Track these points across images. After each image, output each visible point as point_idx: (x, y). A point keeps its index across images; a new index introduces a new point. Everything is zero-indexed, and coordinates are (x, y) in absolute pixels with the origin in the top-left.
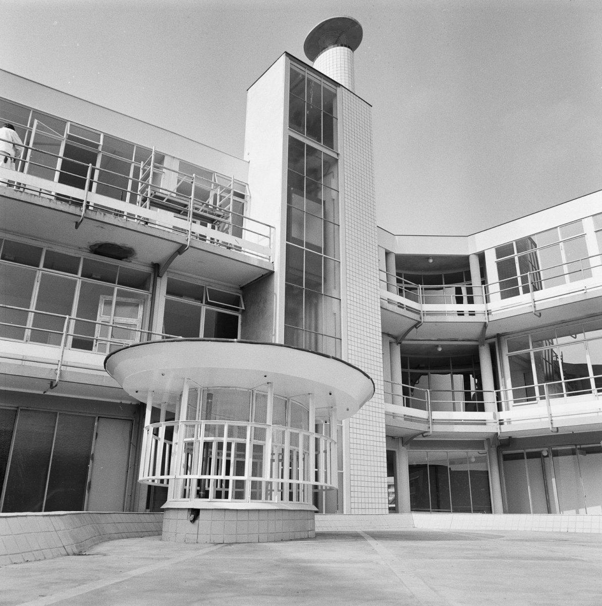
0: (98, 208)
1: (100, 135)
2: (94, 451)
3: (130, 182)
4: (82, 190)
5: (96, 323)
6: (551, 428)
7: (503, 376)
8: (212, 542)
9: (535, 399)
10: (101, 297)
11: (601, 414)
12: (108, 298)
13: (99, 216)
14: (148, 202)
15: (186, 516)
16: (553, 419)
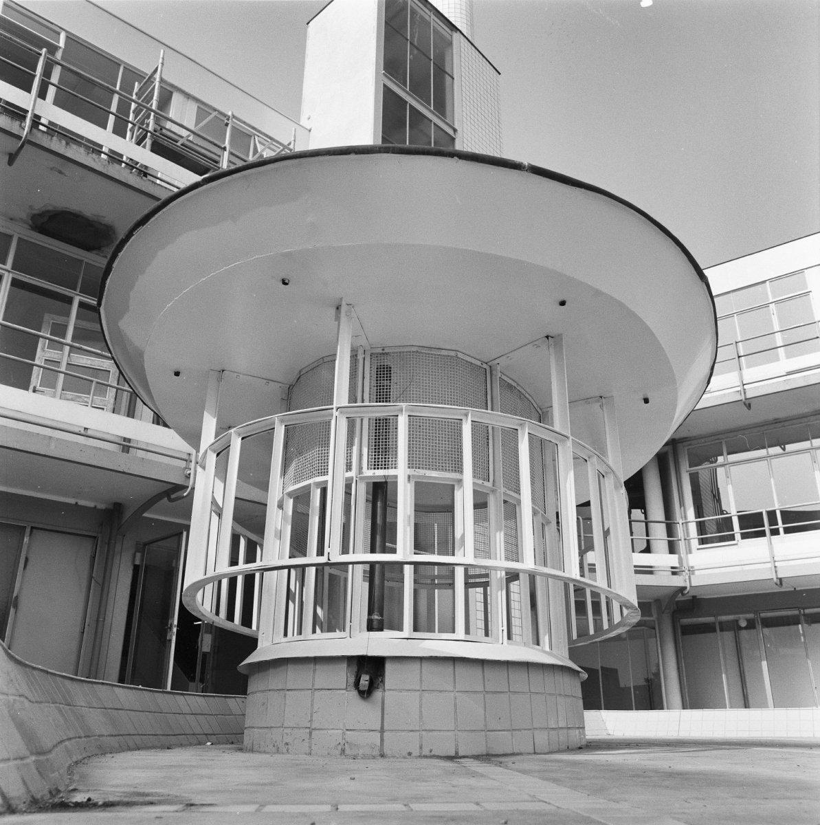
0: (53, 130)
1: (59, 34)
2: (21, 588)
3: (116, 98)
4: (26, 93)
5: (33, 365)
6: (775, 579)
7: (682, 503)
8: (426, 752)
9: (732, 538)
10: (47, 317)
11: (818, 560)
12: (60, 320)
13: (57, 145)
14: (148, 141)
15: (343, 675)
16: (777, 564)
